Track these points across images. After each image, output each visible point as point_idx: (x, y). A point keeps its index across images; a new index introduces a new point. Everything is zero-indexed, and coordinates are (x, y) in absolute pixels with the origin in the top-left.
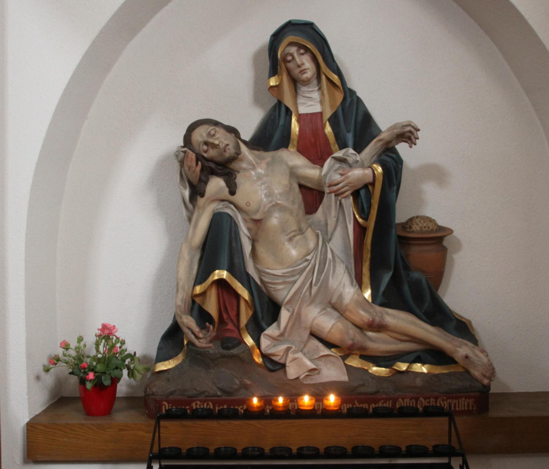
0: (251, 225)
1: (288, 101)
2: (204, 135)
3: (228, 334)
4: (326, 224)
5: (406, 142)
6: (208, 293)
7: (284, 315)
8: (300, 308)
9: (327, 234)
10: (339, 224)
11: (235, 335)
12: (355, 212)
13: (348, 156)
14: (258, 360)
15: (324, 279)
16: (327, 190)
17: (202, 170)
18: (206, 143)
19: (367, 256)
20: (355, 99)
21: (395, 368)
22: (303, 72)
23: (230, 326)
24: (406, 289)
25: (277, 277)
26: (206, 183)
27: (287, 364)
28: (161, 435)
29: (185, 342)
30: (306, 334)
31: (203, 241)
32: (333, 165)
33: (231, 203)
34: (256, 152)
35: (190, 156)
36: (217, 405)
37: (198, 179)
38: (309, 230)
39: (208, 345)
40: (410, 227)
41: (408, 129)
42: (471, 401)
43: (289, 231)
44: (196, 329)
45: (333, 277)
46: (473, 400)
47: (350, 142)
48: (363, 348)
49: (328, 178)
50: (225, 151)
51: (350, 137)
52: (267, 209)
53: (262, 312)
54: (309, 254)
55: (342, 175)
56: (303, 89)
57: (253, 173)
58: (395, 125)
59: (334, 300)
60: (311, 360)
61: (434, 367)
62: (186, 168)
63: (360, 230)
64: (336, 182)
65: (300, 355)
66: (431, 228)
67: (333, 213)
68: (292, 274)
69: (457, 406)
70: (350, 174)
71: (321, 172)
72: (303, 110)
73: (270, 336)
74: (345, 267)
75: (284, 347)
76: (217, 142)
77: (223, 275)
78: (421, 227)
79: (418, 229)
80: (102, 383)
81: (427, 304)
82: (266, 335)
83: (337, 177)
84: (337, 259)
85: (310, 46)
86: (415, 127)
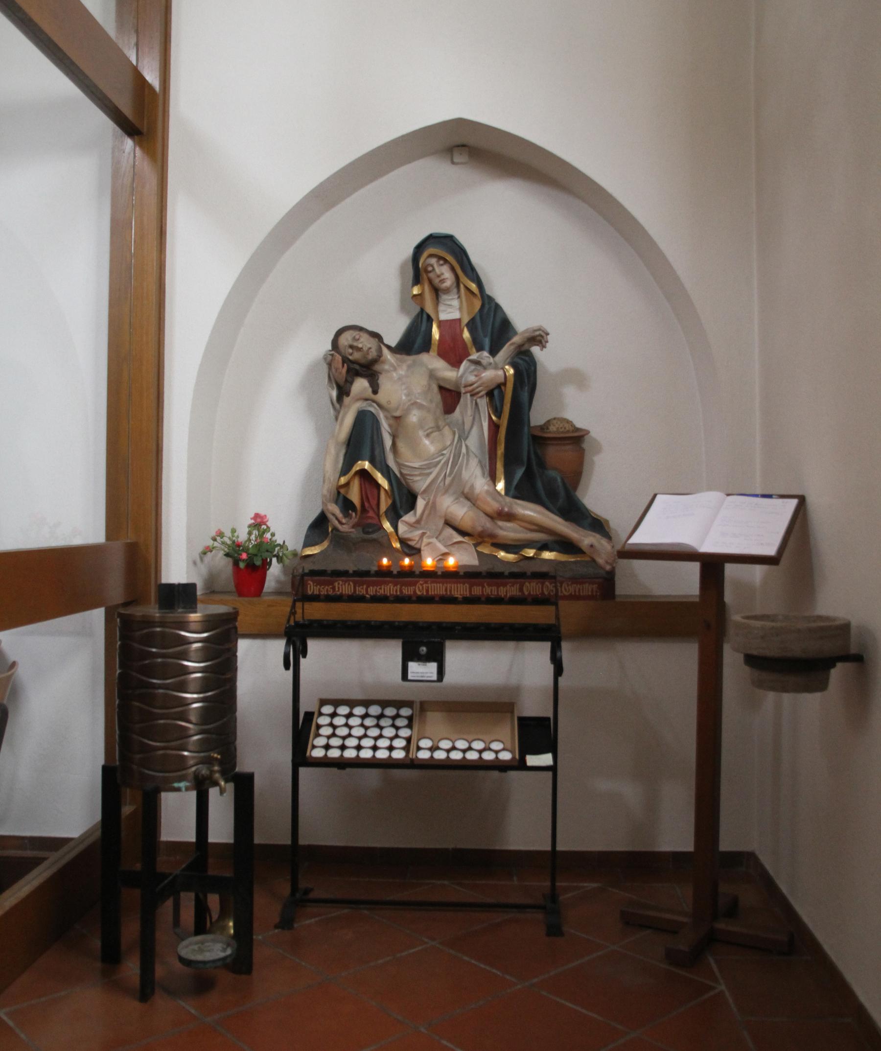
0: (392, 421)
1: (429, 309)
2: (350, 339)
3: (370, 521)
4: (463, 423)
5: (538, 345)
6: (351, 484)
7: (420, 503)
8: (435, 497)
9: (464, 433)
10: (475, 423)
11: (375, 521)
12: (491, 412)
13: (482, 358)
14: (397, 545)
15: (457, 470)
16: (463, 390)
17: (348, 371)
18: (351, 347)
19: (501, 450)
20: (493, 305)
21: (523, 554)
22: (443, 281)
23: (371, 514)
24: (539, 484)
25: (414, 469)
26: (351, 383)
27: (422, 548)
28: (305, 611)
29: (330, 529)
30: (441, 522)
31: (348, 437)
32: (468, 368)
33: (374, 401)
34: (398, 356)
35: (336, 358)
36: (357, 585)
37: (344, 380)
38: (447, 428)
39: (350, 530)
40: (548, 428)
41: (537, 333)
42: (595, 586)
43: (427, 428)
44: (340, 515)
45: (466, 468)
46: (597, 585)
47: (487, 347)
48: (492, 536)
49: (463, 379)
50: (368, 354)
51: (487, 342)
52: (406, 407)
53: (401, 502)
54: (445, 449)
55: (476, 376)
56: (444, 297)
57: (395, 375)
58: (527, 329)
59: (466, 490)
60: (445, 546)
61: (562, 555)
62: (333, 370)
63: (494, 428)
64: (470, 383)
65: (434, 540)
66: (567, 429)
67: (469, 412)
68: (429, 466)
69: (581, 591)
70: (483, 375)
71: (458, 374)
72: (443, 316)
73: (406, 523)
74: (478, 460)
75: (419, 532)
76: (360, 346)
77: (365, 465)
78: (558, 428)
79: (555, 429)
80: (254, 564)
81: (561, 502)
82: (403, 521)
83: (472, 378)
84: (471, 454)
85: (449, 258)
86: (545, 331)
